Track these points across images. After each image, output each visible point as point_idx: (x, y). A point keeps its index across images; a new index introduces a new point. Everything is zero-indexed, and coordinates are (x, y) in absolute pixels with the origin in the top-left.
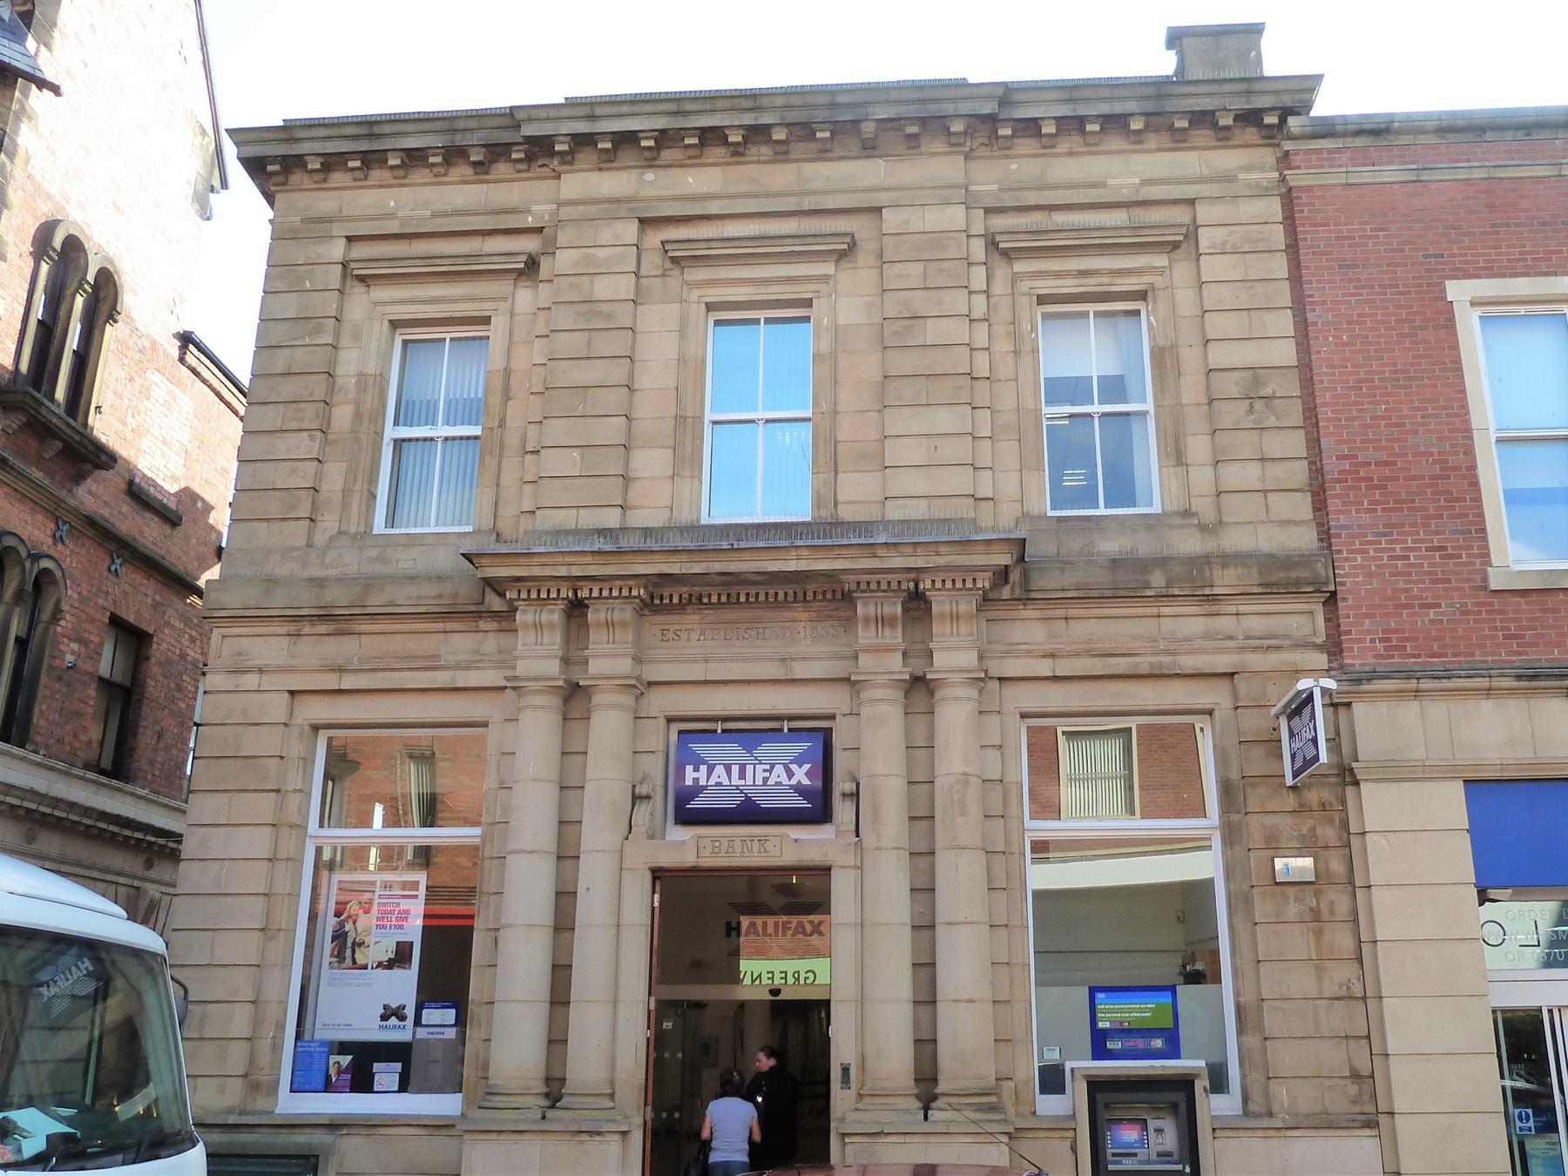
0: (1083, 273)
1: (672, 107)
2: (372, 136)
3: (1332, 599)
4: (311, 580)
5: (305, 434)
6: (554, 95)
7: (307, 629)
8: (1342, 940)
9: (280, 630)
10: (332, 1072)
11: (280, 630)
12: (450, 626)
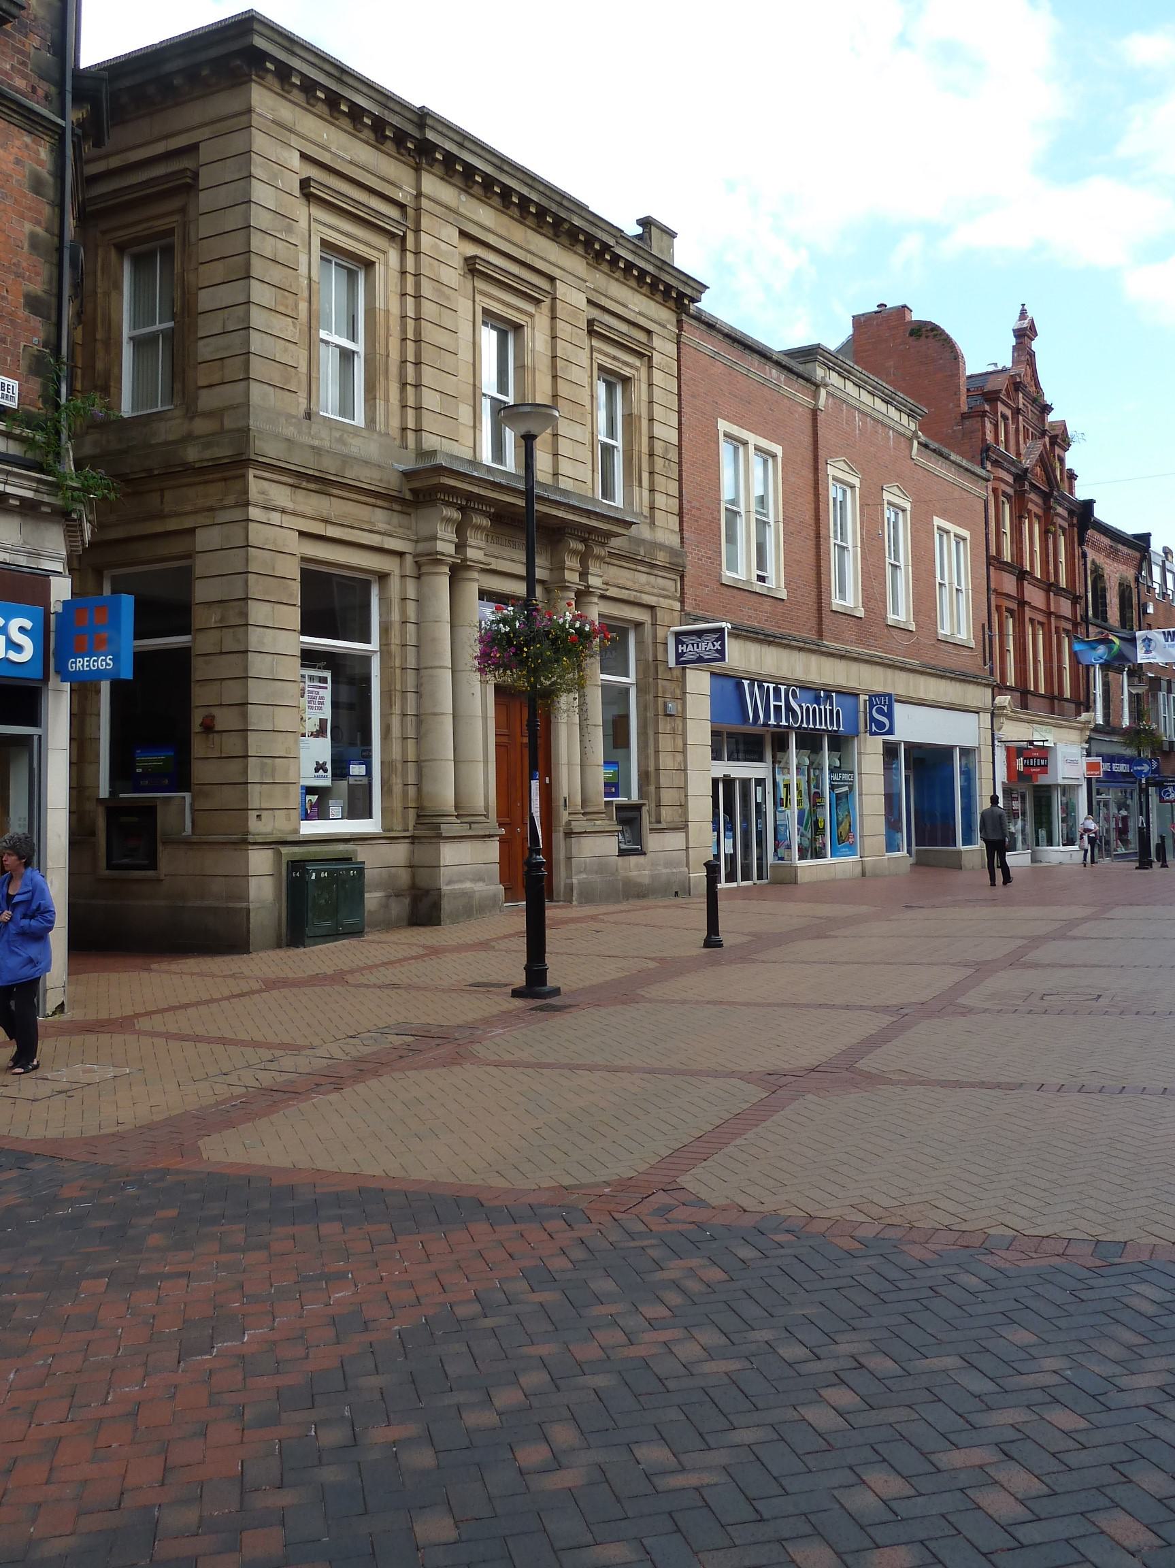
0: (615, 358)
1: (659, 264)
2: (340, 81)
3: (682, 577)
4: (313, 447)
5: (289, 320)
6: (415, 98)
7: (304, 484)
8: (680, 742)
9: (289, 481)
10: (308, 806)
11: (289, 481)
12: (380, 503)
